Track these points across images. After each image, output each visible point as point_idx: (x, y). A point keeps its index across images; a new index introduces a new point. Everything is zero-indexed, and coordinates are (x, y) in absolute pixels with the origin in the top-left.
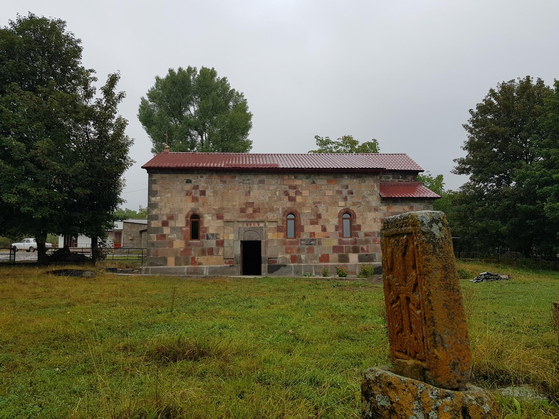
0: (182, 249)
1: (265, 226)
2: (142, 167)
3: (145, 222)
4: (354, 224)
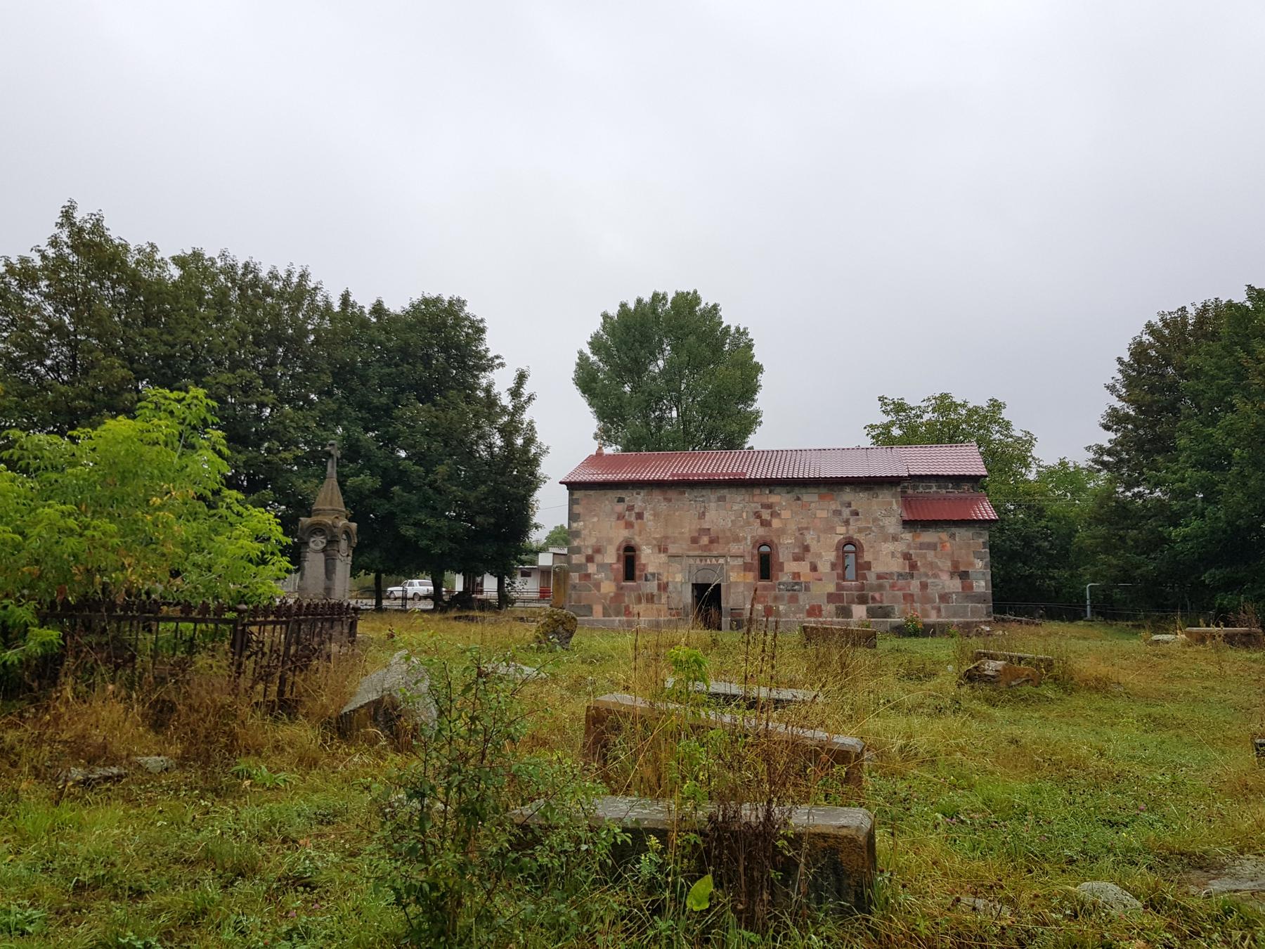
3: (565, 551)
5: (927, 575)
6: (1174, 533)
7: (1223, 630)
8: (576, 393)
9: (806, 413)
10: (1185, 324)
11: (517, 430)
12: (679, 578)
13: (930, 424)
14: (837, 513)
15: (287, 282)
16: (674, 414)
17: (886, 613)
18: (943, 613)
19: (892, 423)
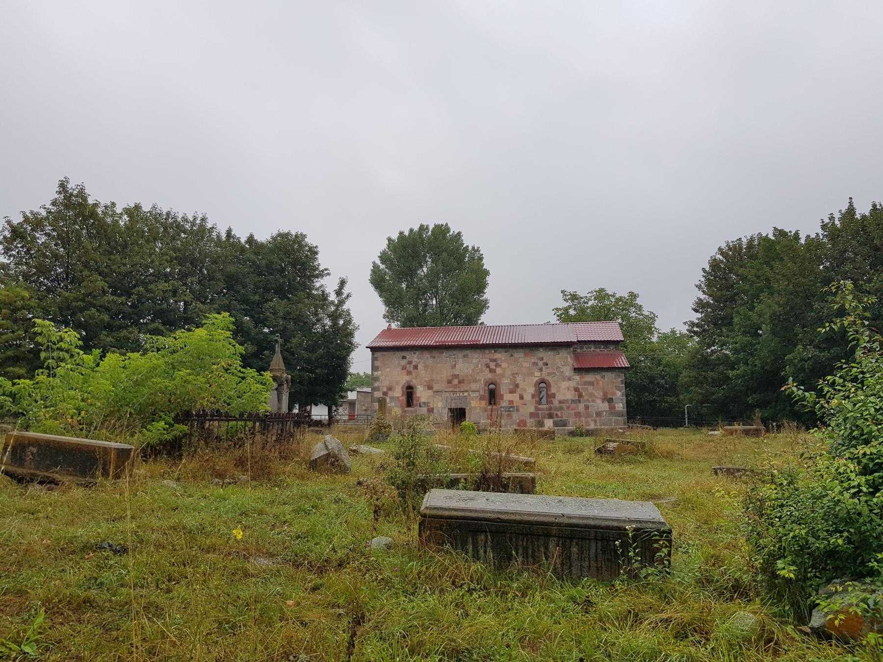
3: (369, 390)
5: (588, 401)
6: (731, 373)
7: (741, 427)
8: (371, 288)
9: (517, 302)
10: (741, 248)
11: (340, 316)
12: (440, 405)
13: (592, 307)
14: (535, 364)
15: (193, 224)
16: (434, 302)
17: (564, 424)
18: (598, 423)
19: (570, 307)
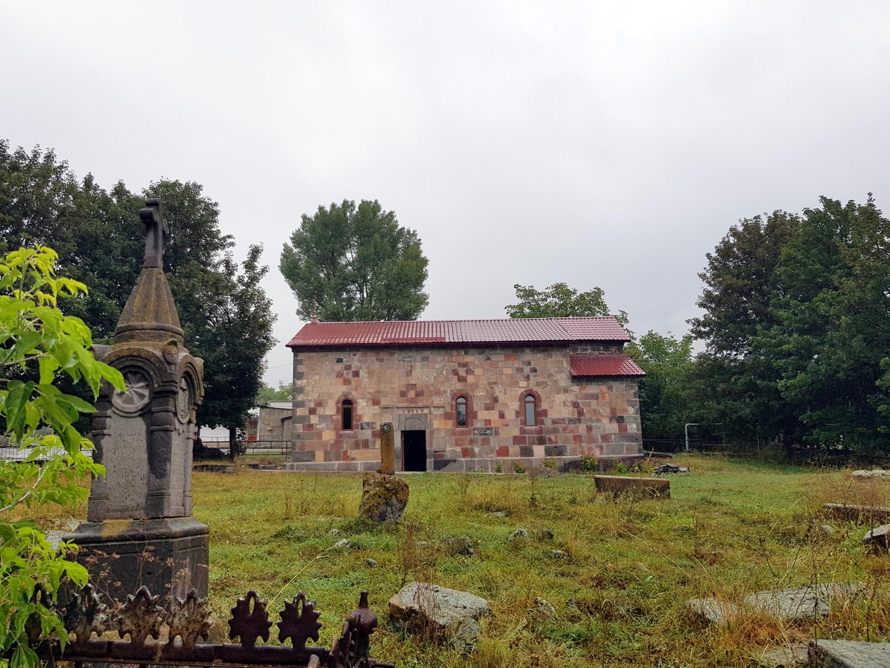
0: (332, 442)
1: (430, 412)
2: (287, 346)
3: (289, 406)
4: (225, 451)
5: (591, 420)
9: (460, 293)
17: (560, 452)
18: (605, 451)
